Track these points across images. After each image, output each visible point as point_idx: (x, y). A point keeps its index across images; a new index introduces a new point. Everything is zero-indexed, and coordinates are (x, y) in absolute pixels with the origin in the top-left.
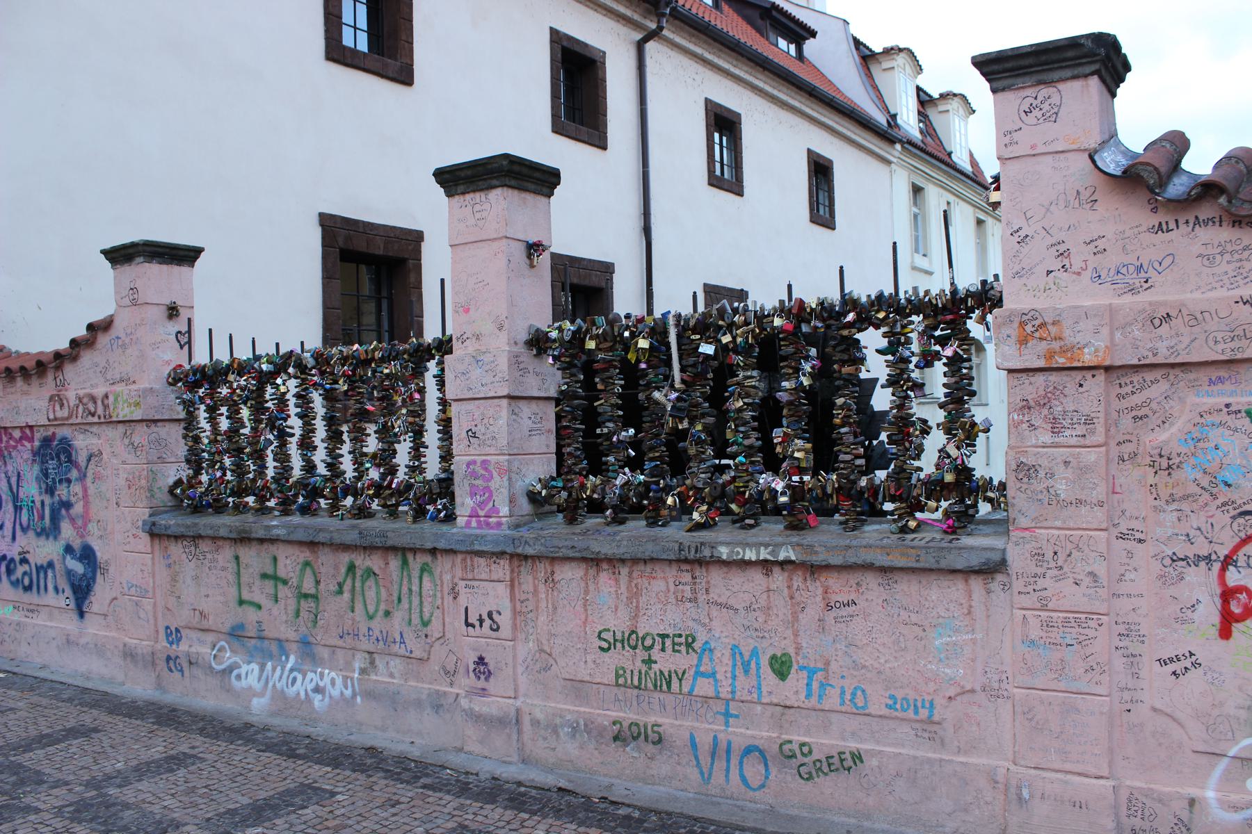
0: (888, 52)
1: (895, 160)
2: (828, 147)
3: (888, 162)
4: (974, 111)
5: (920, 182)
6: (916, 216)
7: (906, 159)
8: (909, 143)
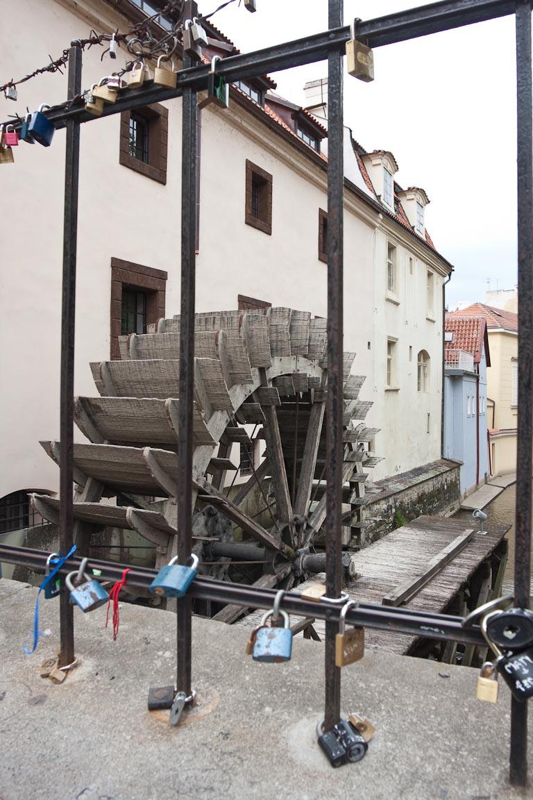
0: (377, 153)
1: (378, 225)
2: (266, 163)
3: (373, 227)
4: (429, 202)
5: (394, 243)
6: (389, 265)
7: (387, 227)
8: (387, 215)
